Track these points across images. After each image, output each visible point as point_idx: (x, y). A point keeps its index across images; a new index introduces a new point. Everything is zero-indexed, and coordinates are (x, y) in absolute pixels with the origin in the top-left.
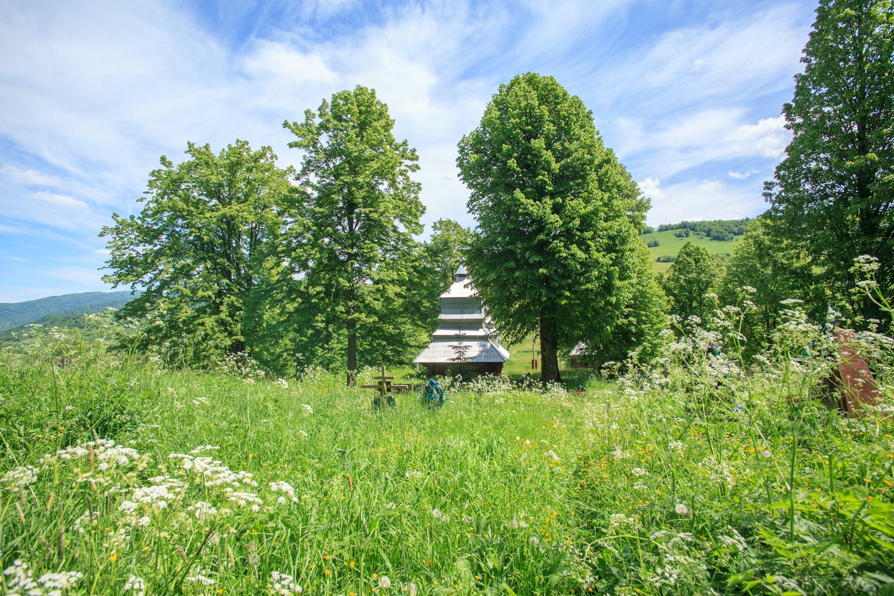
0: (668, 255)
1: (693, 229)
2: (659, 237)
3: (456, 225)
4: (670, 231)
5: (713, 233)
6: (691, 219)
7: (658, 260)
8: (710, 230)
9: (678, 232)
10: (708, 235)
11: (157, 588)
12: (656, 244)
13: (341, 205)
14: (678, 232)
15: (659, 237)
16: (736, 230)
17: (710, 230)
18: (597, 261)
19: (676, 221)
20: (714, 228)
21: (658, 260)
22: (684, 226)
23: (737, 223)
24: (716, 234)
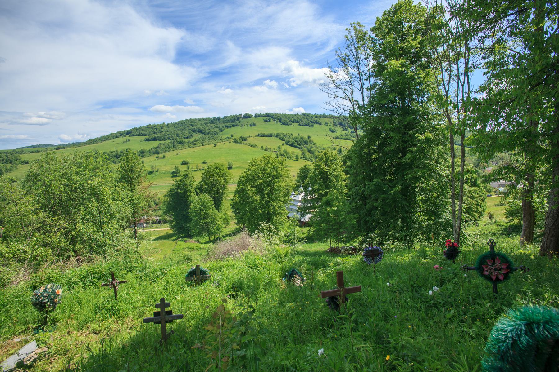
0: (263, 133)
1: (272, 118)
2: (256, 121)
3: (219, 119)
4: (260, 118)
5: (283, 121)
6: (271, 112)
7: (259, 135)
8: (281, 119)
9: (265, 118)
10: (280, 122)
11: (1, 322)
12: (254, 125)
13: (419, 198)
14: (265, 118)
15: (256, 121)
16: (292, 120)
17: (281, 119)
18: (237, 192)
19: (264, 112)
20: (283, 118)
21: (259, 135)
22: (268, 115)
23: (94, 140)
24: (284, 122)
